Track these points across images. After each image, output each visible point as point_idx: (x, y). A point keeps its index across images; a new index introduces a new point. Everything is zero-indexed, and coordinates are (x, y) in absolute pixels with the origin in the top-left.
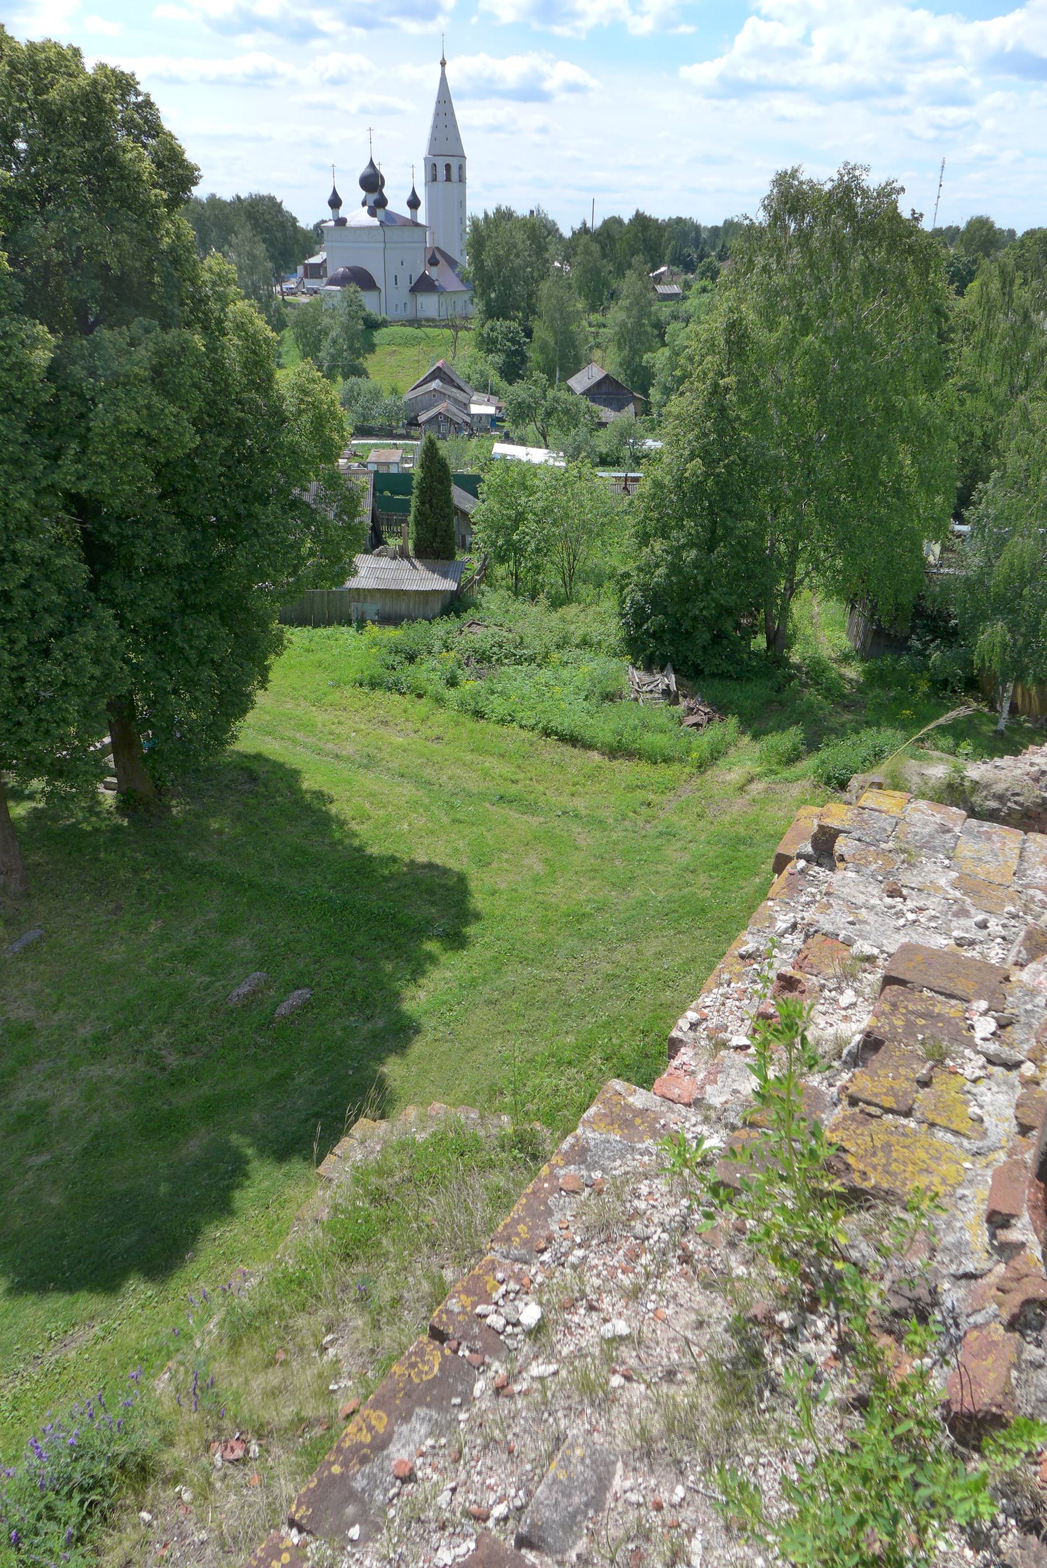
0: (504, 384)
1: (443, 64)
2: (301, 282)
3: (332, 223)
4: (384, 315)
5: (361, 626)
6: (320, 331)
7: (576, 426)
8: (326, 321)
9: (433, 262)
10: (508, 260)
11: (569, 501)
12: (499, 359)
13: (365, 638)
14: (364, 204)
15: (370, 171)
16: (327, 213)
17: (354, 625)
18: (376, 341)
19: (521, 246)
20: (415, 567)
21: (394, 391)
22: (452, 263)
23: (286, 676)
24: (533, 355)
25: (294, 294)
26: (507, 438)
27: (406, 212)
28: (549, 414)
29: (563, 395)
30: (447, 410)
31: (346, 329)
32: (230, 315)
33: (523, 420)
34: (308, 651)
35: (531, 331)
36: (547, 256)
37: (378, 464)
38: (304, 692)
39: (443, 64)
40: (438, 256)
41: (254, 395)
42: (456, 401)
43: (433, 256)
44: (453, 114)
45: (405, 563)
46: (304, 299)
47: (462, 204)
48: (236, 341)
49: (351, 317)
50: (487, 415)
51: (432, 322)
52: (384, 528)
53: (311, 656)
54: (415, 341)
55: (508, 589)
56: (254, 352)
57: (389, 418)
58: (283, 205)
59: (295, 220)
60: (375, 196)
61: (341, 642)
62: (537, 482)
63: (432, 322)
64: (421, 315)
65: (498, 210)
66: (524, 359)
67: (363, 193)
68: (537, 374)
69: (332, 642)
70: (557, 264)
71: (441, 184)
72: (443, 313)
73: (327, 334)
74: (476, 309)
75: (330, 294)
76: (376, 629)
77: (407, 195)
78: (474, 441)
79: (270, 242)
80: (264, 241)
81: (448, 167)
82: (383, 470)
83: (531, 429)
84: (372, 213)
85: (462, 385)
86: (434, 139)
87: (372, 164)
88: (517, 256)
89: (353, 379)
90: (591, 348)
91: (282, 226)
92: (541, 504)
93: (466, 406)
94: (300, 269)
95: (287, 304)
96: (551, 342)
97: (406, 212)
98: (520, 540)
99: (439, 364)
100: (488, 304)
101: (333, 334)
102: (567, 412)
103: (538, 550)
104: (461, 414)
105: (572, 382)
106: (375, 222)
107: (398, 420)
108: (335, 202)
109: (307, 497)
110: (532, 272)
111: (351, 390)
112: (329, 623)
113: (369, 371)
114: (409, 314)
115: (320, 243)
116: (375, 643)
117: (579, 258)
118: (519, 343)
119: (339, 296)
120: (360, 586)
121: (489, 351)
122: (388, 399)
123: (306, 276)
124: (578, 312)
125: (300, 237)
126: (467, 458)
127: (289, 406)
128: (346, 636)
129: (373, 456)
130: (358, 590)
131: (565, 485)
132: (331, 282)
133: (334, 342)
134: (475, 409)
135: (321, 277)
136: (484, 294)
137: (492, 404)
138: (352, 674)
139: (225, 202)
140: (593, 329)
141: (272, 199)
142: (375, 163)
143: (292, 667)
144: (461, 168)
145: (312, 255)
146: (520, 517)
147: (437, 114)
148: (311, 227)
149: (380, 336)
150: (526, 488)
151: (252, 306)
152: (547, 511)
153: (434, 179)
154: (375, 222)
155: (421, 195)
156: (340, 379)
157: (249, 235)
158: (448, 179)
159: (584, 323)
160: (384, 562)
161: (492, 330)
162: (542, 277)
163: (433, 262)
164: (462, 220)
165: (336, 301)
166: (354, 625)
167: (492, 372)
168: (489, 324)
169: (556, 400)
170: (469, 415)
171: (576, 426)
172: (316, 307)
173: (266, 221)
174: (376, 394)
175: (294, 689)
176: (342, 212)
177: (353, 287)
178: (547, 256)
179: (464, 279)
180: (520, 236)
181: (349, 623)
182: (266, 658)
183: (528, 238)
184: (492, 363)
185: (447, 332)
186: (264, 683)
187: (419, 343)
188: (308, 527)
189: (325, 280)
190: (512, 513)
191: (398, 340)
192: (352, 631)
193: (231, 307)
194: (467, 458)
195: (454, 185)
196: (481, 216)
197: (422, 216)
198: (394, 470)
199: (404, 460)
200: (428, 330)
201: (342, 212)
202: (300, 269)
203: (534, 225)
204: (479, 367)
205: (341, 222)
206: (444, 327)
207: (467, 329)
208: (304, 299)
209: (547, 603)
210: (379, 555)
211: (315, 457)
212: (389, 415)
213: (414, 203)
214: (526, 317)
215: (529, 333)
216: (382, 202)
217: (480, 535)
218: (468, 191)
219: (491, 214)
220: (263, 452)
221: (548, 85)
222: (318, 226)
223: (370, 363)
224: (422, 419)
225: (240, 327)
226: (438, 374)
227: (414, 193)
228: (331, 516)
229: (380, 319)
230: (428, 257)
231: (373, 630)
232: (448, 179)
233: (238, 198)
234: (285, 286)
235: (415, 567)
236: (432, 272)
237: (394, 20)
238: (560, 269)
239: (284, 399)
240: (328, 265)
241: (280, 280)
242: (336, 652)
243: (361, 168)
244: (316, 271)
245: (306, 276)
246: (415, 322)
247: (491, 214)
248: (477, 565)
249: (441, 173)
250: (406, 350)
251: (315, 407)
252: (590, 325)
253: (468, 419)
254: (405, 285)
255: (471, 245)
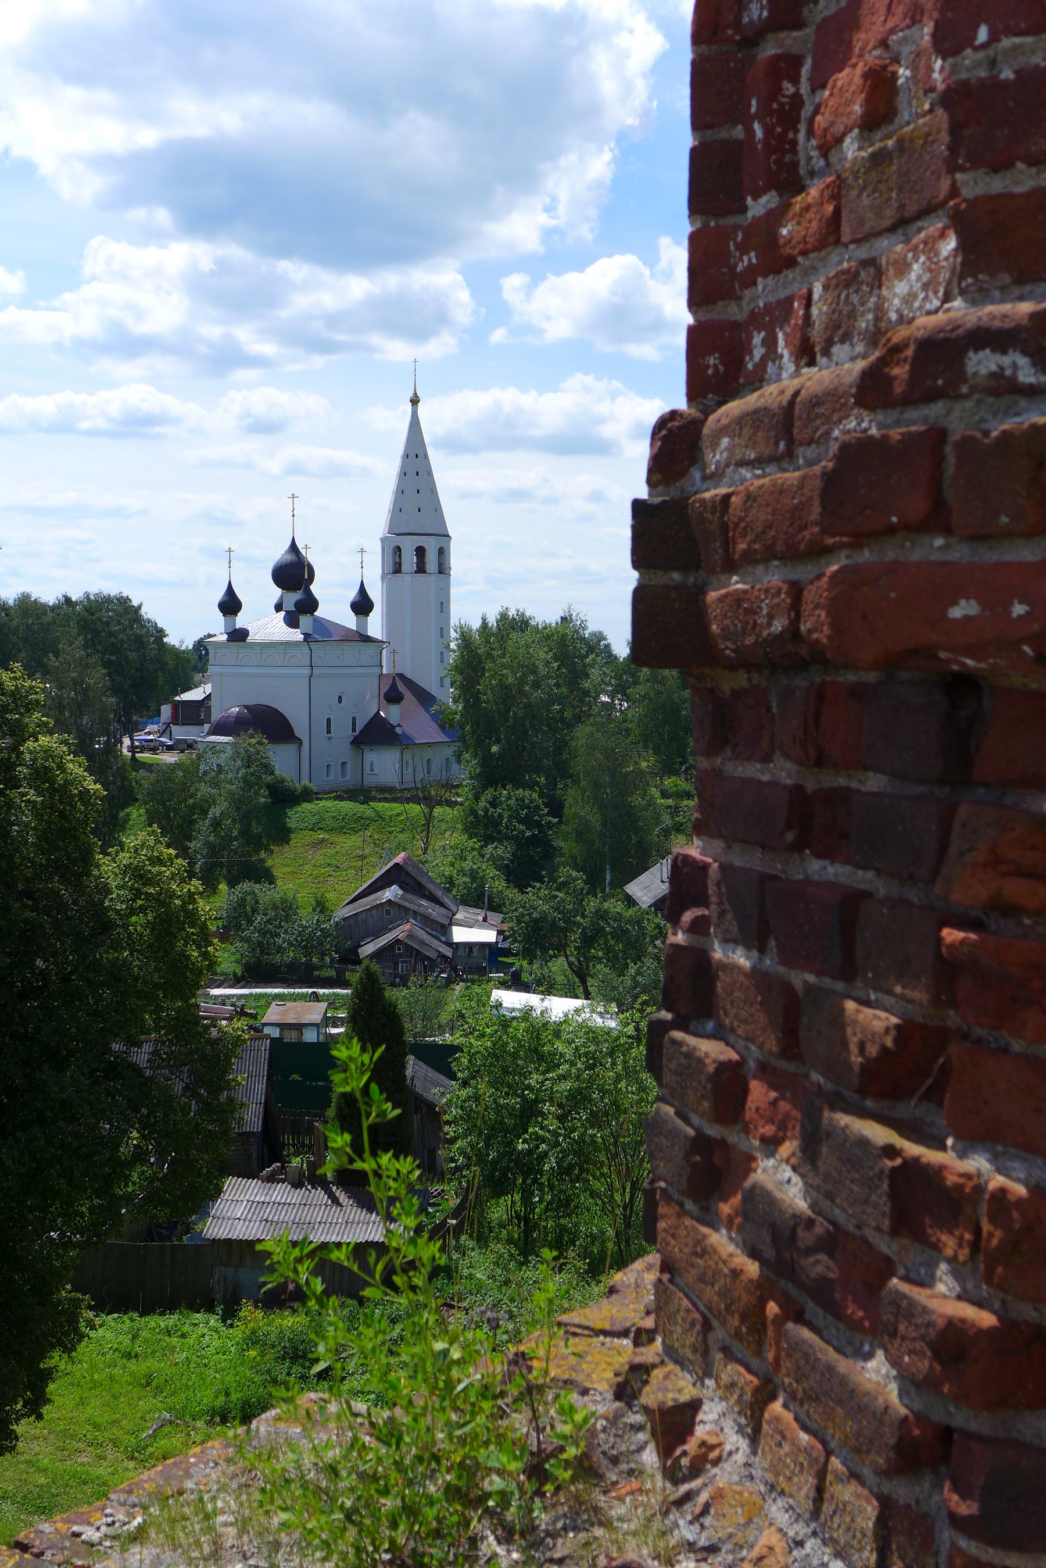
0: (512, 893)
1: (415, 401)
2: (165, 731)
3: (225, 637)
4: (305, 782)
5: (229, 1315)
6: (194, 806)
7: (638, 959)
8: (204, 790)
9: (393, 697)
10: (521, 692)
11: (618, 1079)
12: (502, 851)
13: (238, 1333)
14: (278, 608)
15: (290, 558)
16: (216, 626)
17: (219, 1309)
18: (291, 824)
19: (542, 670)
20: (335, 1201)
21: (321, 906)
22: (425, 698)
23: (82, 1402)
24: (565, 844)
25: (154, 750)
26: (516, 983)
27: (349, 620)
28: (589, 940)
29: (613, 906)
30: (411, 936)
31: (237, 802)
32: (27, 757)
33: (544, 950)
34: (128, 1356)
35: (561, 806)
36: (586, 685)
37: (282, 1026)
38: (116, 1433)
39: (415, 401)
40: (401, 687)
41: (56, 884)
42: (427, 921)
43: (394, 687)
44: (430, 473)
45: (319, 1195)
46: (169, 758)
47: (443, 607)
48: (32, 795)
49: (248, 783)
50: (483, 945)
51: (388, 793)
52: (288, 1139)
53: (132, 1365)
54: (359, 824)
55: (510, 1241)
56: (62, 815)
57: (308, 951)
58: (143, 611)
59: (161, 633)
60: (297, 596)
61: (191, 1341)
62: (560, 1046)
63: (388, 793)
64: (369, 780)
65: (503, 617)
66: (549, 852)
67: (276, 592)
68: (565, 872)
69: (174, 1341)
70: (605, 698)
71: (408, 578)
72: (408, 777)
73: (205, 812)
74: (464, 773)
75: (213, 746)
76: (259, 1314)
77: (352, 594)
78: (459, 988)
79: (114, 669)
80: (107, 664)
81: (420, 552)
82: (291, 1037)
83: (558, 966)
84: (292, 621)
85: (439, 893)
86: (398, 510)
87: (294, 547)
88: (536, 685)
89: (246, 886)
90: (666, 833)
91: (140, 642)
92: (567, 1085)
93: (444, 930)
94: (166, 710)
95: (135, 762)
96: (595, 820)
97: (349, 620)
98: (530, 1152)
99: (399, 859)
100: (487, 760)
101: (215, 811)
102: (620, 934)
103: (564, 1171)
104: (436, 944)
105: (634, 888)
106: (297, 635)
107: (323, 955)
108: (230, 605)
109: (141, 1056)
110: (561, 711)
111: (242, 902)
112: (167, 1305)
113: (276, 872)
114: (350, 779)
115: (203, 670)
116: (253, 1340)
117: (641, 689)
118: (538, 825)
119: (229, 750)
120: (234, 1235)
121: (488, 839)
122: (306, 917)
123: (175, 720)
124: (641, 773)
125: (168, 659)
126: (444, 1018)
127: (116, 901)
128: (202, 1329)
129: (273, 1014)
130: (228, 1242)
131: (611, 1053)
132: (217, 730)
133: (216, 824)
134: (461, 935)
135: (201, 723)
136: (480, 747)
137: (491, 926)
138: (207, 1397)
139: (44, 606)
140: (670, 802)
141: (123, 602)
142: (300, 545)
143: (96, 1385)
144: (443, 553)
145: (187, 688)
146: (530, 1112)
147: (403, 474)
148: (189, 644)
149: (298, 815)
150: (541, 1058)
151: (65, 742)
152: (578, 1098)
153: (397, 569)
154: (297, 635)
155: (375, 594)
156: (223, 887)
157: (80, 653)
158: (421, 569)
159: (655, 792)
160: (280, 1192)
161: (494, 804)
162: (578, 719)
163: (393, 697)
164: (443, 632)
165: (222, 759)
166: (219, 1309)
167: (492, 872)
168: (489, 794)
169: (602, 915)
170: (450, 944)
171: (638, 959)
172: (190, 771)
173: (112, 634)
174: (286, 909)
175: (97, 1427)
176: (241, 620)
177: (251, 740)
178: (586, 685)
179: (444, 722)
180: (542, 655)
181: (210, 1309)
182: (43, 1357)
183: (556, 658)
184: (492, 858)
185: (415, 809)
186: (35, 1407)
187: (366, 827)
188: (136, 1109)
189: (207, 727)
190: (515, 1101)
191: (331, 823)
192: (214, 1321)
193: (30, 744)
194: (444, 1018)
195: (429, 580)
196: (476, 624)
197: (375, 625)
198: (310, 1036)
199: (329, 1021)
200: (380, 806)
201: (241, 620)
202: (166, 710)
203: (565, 635)
204: (467, 865)
205: (238, 636)
206: (409, 800)
207: (451, 804)
208: (169, 758)
209: (582, 1266)
210: (272, 1179)
211: (157, 986)
212: (309, 943)
213: (362, 606)
214: (552, 784)
215: (556, 808)
216: (309, 605)
217: (459, 1143)
218: (454, 591)
219: (492, 621)
220: (65, 979)
221: (608, 431)
222: (200, 644)
223: (278, 861)
224: (368, 949)
225: (42, 776)
226: (395, 875)
227: (362, 590)
228: (178, 1087)
229: (299, 787)
230: (385, 688)
231: (250, 1315)
232: (421, 569)
233: (68, 600)
234: (140, 736)
235: (335, 1201)
236: (392, 714)
237: (375, 339)
238: (609, 707)
239: (108, 891)
240: (214, 703)
241: (131, 729)
242: (180, 1357)
243: (278, 552)
244: (193, 714)
245: (175, 720)
246: (360, 793)
247: (492, 621)
248: (454, 1202)
249: (409, 560)
250: (342, 839)
251: (163, 904)
252: (664, 795)
253: (448, 952)
254: (343, 733)
255: (457, 669)
